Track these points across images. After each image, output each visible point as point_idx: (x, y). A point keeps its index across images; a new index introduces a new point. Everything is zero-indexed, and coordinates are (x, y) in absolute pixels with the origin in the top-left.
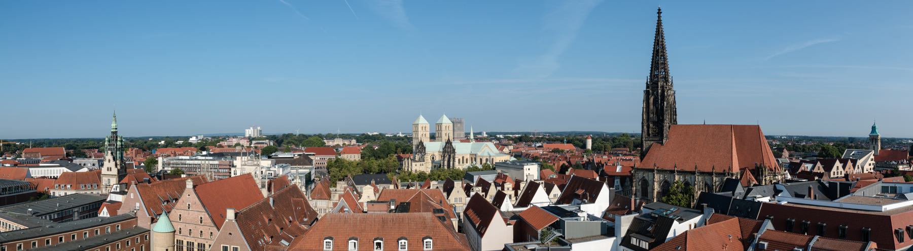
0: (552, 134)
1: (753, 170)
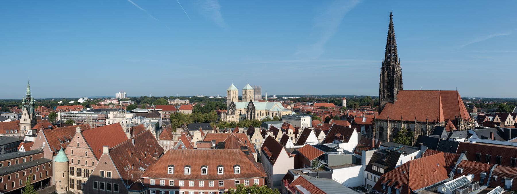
0: (320, 96)
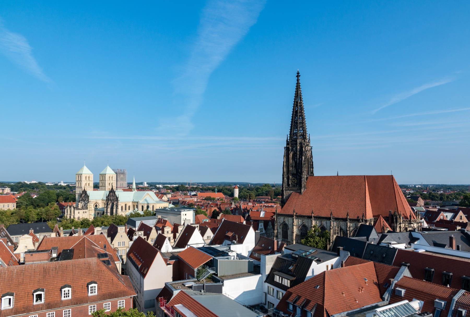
0: (203, 184)
1: (387, 217)
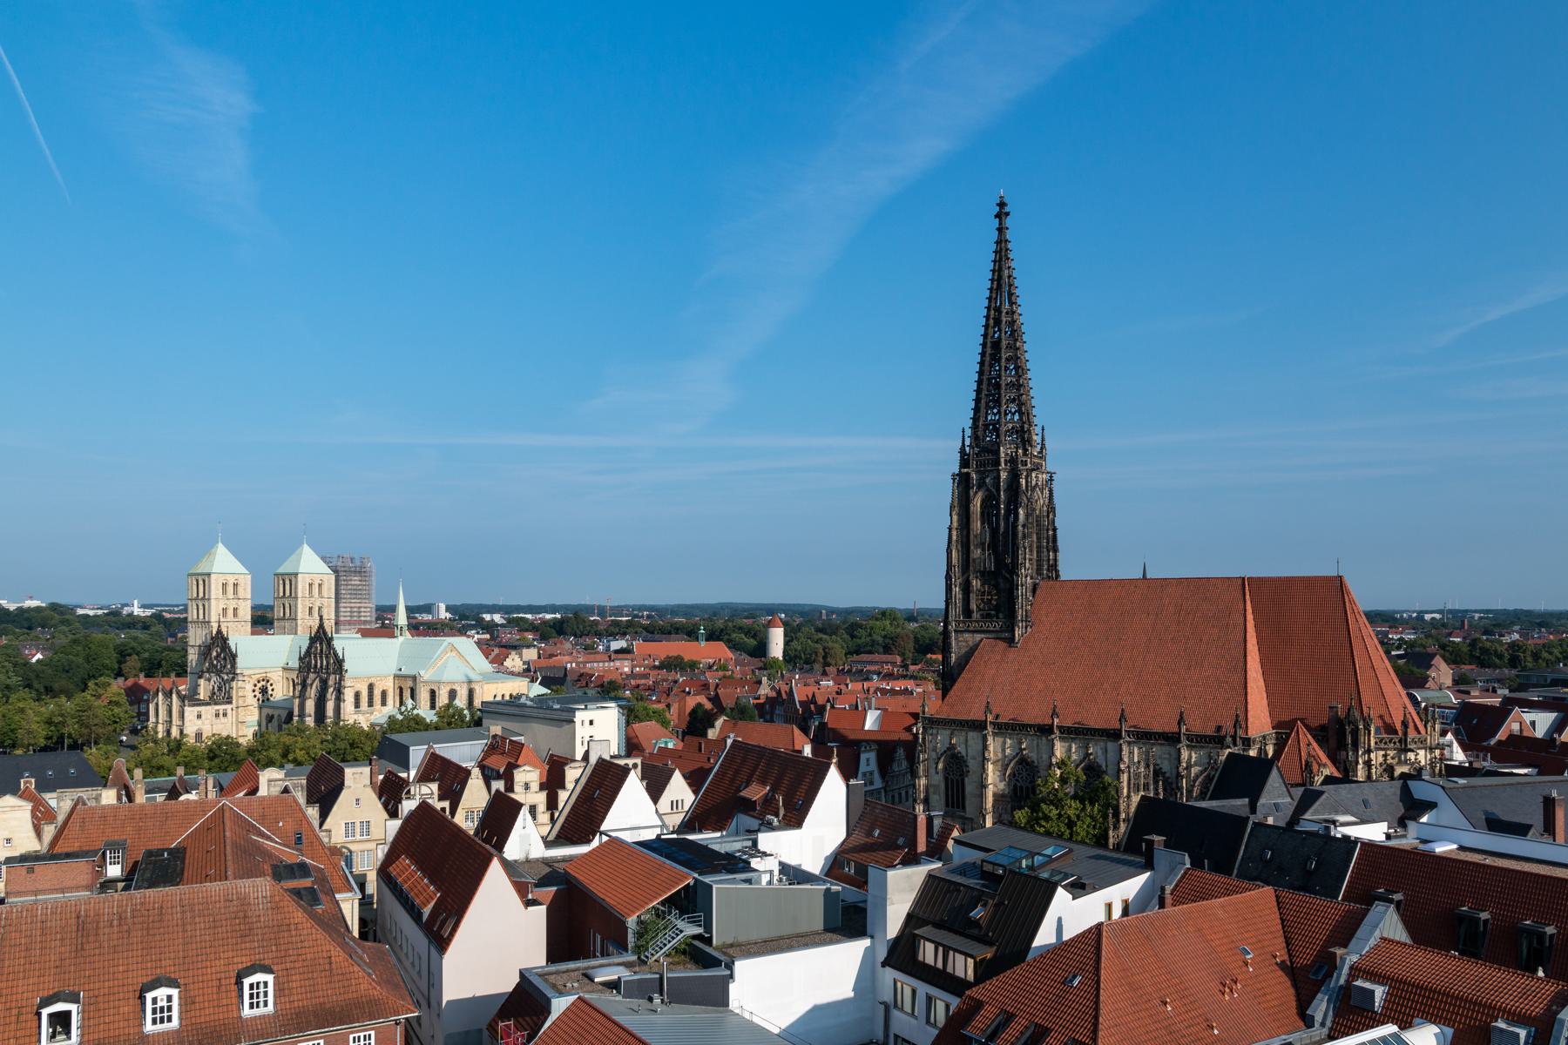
0: (661, 611)
1: (1323, 728)
